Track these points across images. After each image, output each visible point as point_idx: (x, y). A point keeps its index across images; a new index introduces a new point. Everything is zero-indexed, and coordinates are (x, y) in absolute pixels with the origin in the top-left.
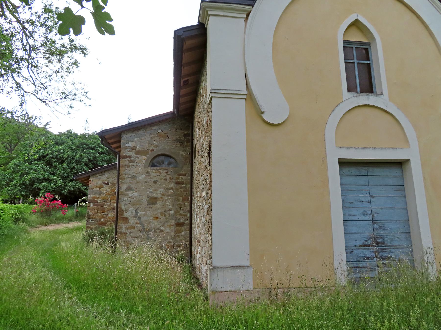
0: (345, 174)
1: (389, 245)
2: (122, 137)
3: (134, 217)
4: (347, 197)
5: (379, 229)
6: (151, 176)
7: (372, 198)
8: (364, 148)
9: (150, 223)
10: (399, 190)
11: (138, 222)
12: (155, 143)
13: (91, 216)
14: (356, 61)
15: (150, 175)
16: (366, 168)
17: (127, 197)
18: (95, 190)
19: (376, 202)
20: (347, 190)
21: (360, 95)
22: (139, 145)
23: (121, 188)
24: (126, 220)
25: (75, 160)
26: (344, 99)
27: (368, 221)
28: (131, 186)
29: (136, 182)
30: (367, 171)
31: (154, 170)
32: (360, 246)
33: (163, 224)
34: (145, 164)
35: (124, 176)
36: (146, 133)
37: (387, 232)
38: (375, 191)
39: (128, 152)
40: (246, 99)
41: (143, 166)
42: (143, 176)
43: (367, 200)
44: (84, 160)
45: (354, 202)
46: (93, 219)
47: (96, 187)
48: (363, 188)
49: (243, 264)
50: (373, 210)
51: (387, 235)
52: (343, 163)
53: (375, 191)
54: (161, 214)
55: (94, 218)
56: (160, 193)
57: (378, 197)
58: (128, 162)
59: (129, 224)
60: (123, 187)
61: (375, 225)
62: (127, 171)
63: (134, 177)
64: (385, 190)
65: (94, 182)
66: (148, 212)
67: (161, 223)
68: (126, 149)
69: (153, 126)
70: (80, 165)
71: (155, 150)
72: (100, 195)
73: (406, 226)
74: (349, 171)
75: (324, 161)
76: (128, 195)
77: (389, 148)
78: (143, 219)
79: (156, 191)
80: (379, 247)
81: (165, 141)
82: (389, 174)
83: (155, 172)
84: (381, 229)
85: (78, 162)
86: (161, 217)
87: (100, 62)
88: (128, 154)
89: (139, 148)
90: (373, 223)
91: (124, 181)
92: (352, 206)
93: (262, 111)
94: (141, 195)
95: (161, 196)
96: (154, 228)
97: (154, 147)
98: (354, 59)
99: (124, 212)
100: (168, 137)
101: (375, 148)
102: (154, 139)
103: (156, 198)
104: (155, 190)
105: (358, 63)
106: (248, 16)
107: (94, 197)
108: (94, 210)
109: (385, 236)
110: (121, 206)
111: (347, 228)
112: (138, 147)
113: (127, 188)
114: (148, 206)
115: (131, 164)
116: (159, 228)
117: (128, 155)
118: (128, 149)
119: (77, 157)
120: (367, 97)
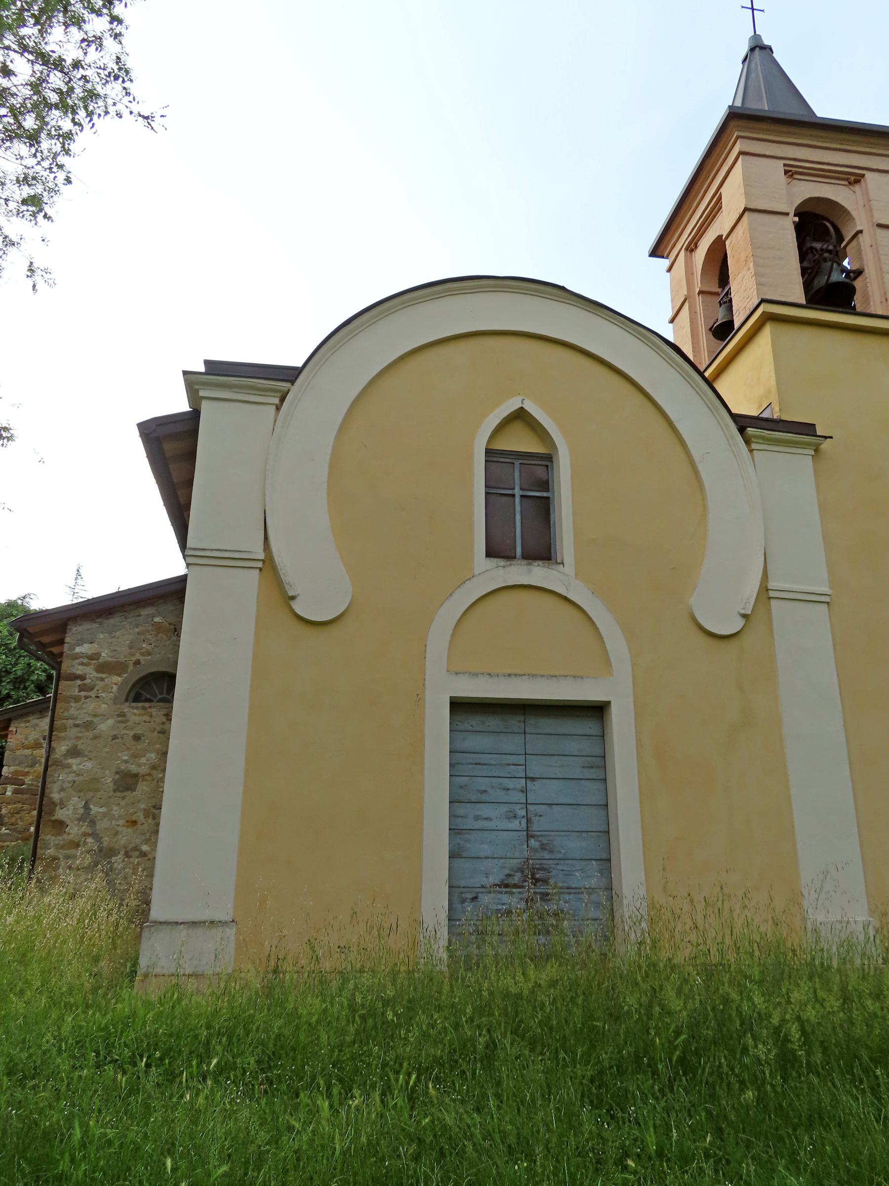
2: (68, 631)
3: (79, 820)
6: (129, 724)
7: (529, 782)
9: (117, 833)
10: (592, 767)
11: (87, 831)
12: (144, 646)
13: (6, 820)
14: (517, 492)
15: (127, 721)
17: (66, 770)
18: (21, 755)
19: (539, 792)
20: (477, 764)
21: (511, 565)
22: (106, 651)
23: (54, 749)
24: (60, 826)
25: (12, 676)
26: (476, 573)
28: (80, 746)
29: (92, 737)
31: (137, 708)
33: (148, 837)
34: (117, 694)
35: (64, 721)
36: (124, 623)
38: (536, 767)
39: (80, 667)
40: (261, 569)
41: (111, 699)
42: (110, 722)
43: (519, 787)
44: (34, 677)
45: (489, 790)
46: (11, 827)
47: (24, 747)
48: (512, 759)
49: (217, 917)
50: (530, 807)
51: (558, 864)
52: (459, 706)
53: (536, 767)
54: (144, 814)
55: (12, 824)
56: (148, 762)
57: (544, 781)
58: (77, 690)
59: (65, 836)
60: (61, 748)
61: (533, 840)
62: (72, 711)
63: (88, 726)
64: (560, 766)
65: (21, 734)
66: (115, 808)
67: (143, 834)
68: (76, 658)
69: (144, 606)
70: (25, 688)
71: (142, 662)
72: (32, 766)
73: (601, 846)
74: (483, 723)
75: (420, 699)
76: (69, 766)
78: (101, 825)
79: (136, 760)
80: (537, 890)
81: (168, 643)
83: (139, 715)
85: (20, 682)
86: (143, 821)
88: (79, 670)
89: (105, 655)
90: (529, 837)
91: (62, 734)
92: (484, 797)
93: (290, 595)
94: (102, 768)
95: (148, 771)
96: (125, 847)
97: (142, 654)
99: (58, 808)
100: (176, 633)
102: (142, 637)
103: (136, 776)
104: (136, 757)
106: (282, 400)
107: (16, 773)
108: (15, 803)
110: (50, 793)
111: (468, 845)
112: (103, 655)
113: (68, 751)
114: (115, 795)
115: (83, 694)
116: (137, 847)
117: (79, 672)
118: (81, 660)
119: (19, 670)
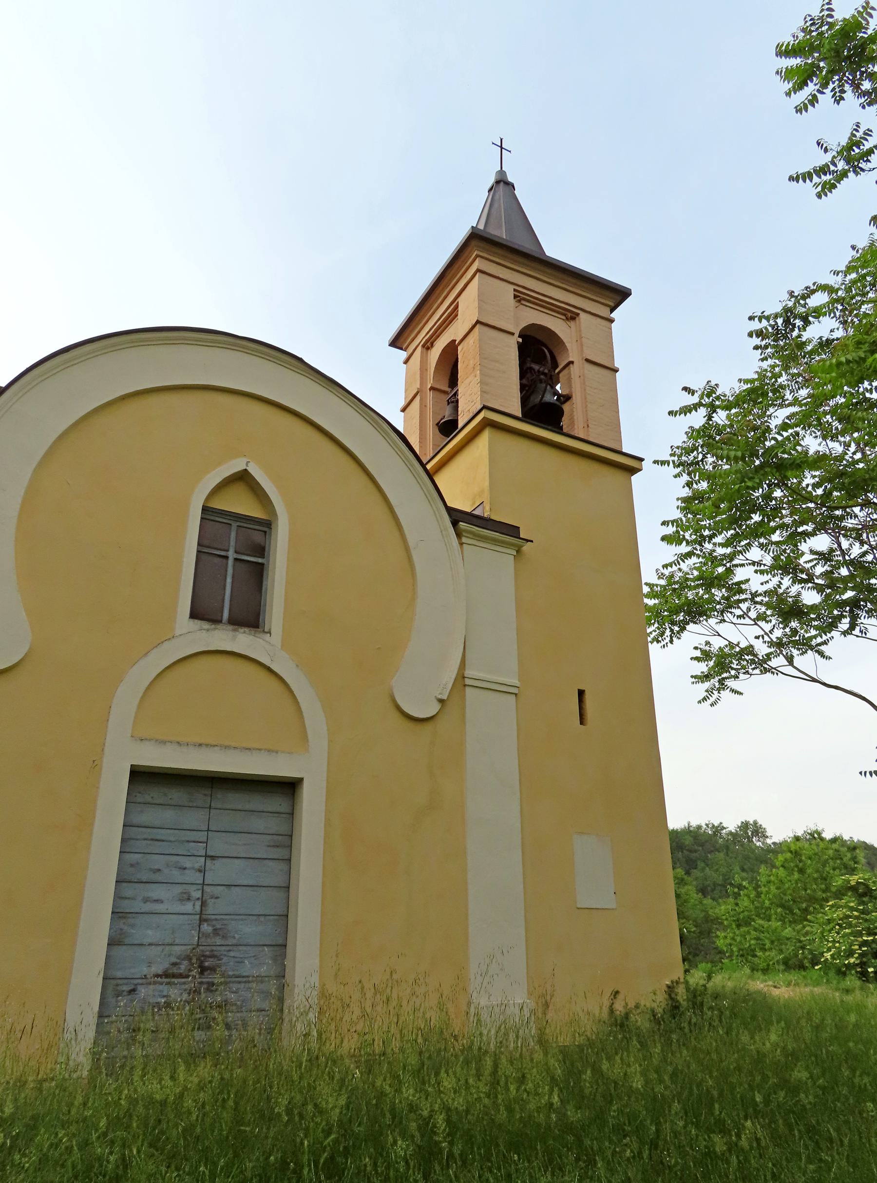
0: (155, 802)
1: (231, 973)
4: (149, 856)
5: (211, 935)
7: (209, 862)
8: (200, 745)
10: (278, 846)
14: (231, 554)
16: (208, 792)
19: (218, 872)
20: (152, 840)
26: (177, 633)
27: (189, 916)
30: (209, 798)
32: (157, 976)
37: (230, 941)
38: (218, 846)
43: (197, 866)
51: (230, 951)
53: (218, 846)
74: (165, 795)
75: (96, 766)
77: (260, 750)
82: (261, 808)
84: (218, 935)
87: (671, 447)
90: (201, 921)
92: (158, 877)
98: (228, 551)
101: (227, 747)
105: (236, 559)
109: (225, 953)
120: (231, 633)
